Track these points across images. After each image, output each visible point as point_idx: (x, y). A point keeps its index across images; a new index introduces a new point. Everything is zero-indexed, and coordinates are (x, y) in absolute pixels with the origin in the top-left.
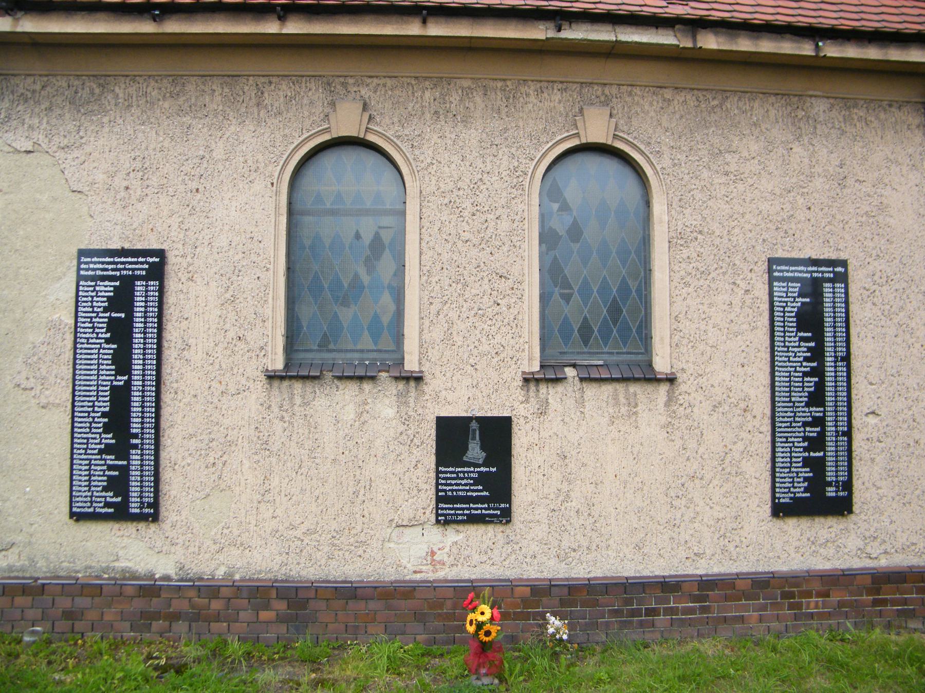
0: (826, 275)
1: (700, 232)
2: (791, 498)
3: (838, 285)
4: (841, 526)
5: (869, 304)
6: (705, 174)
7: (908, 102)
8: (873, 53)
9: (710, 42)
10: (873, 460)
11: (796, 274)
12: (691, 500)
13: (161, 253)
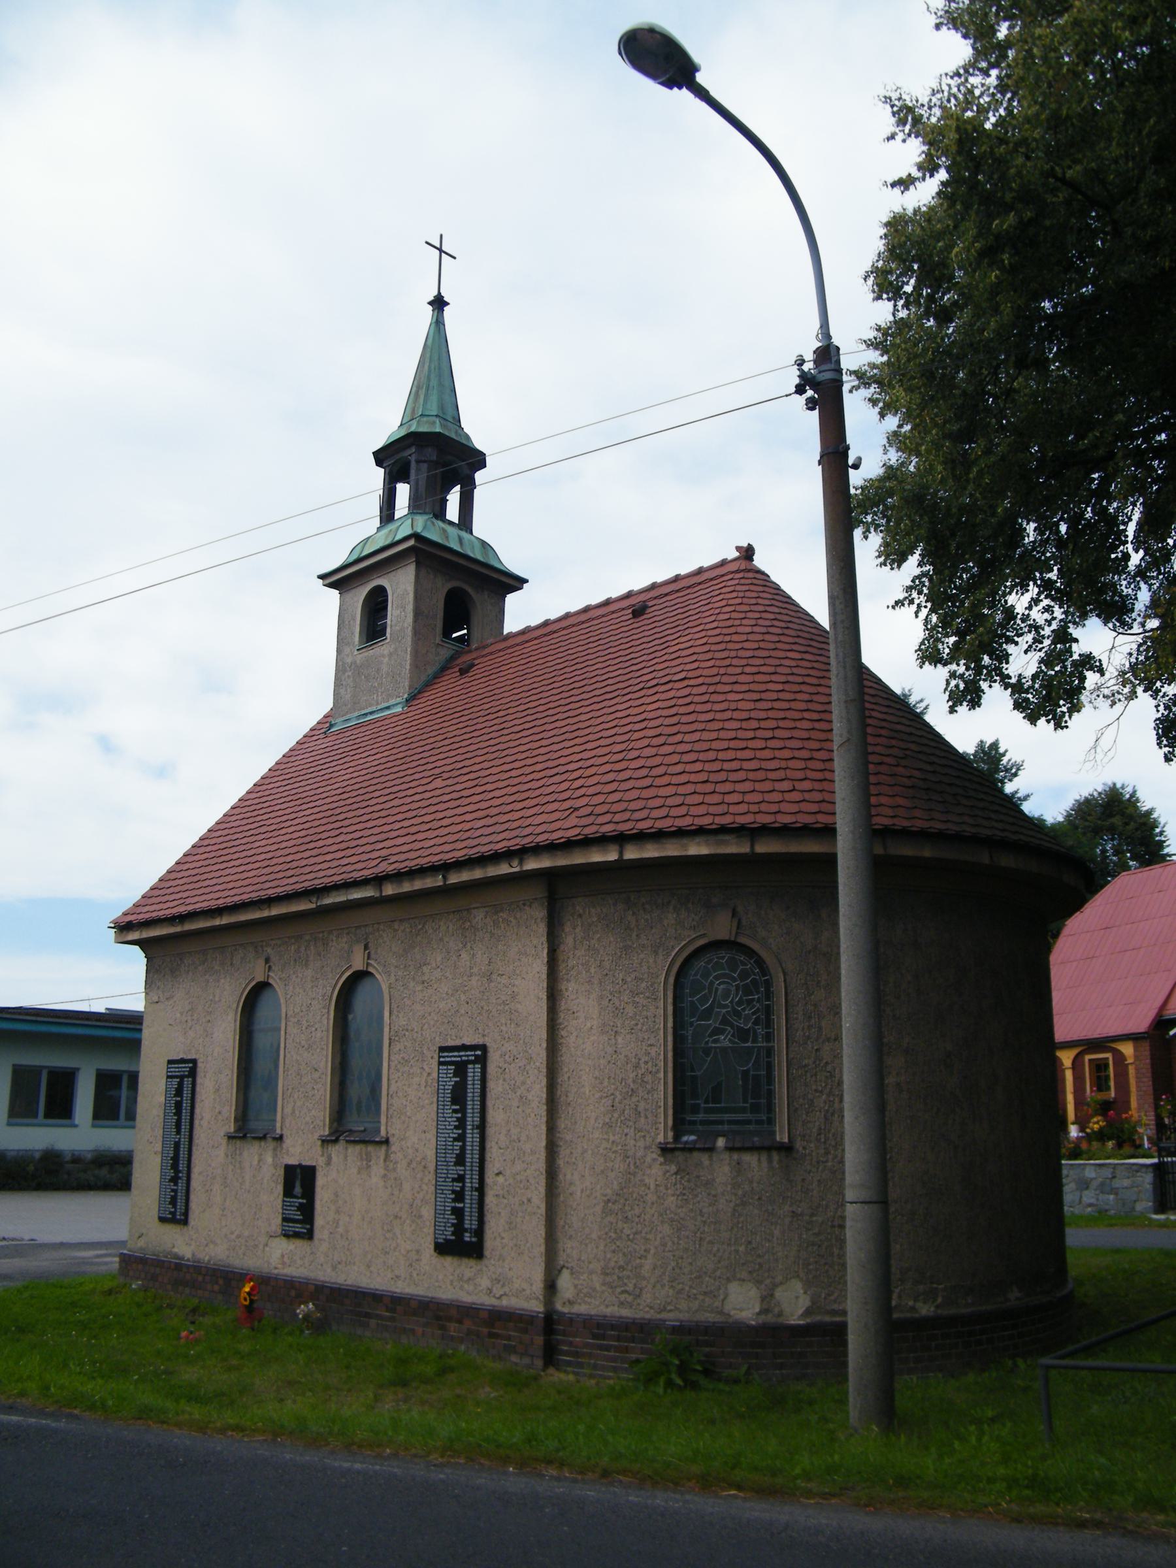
0: (470, 1058)
1: (407, 1030)
2: (445, 1239)
3: (477, 1066)
4: (478, 1268)
5: (501, 1081)
6: (412, 984)
7: (536, 899)
8: (478, 874)
9: (389, 890)
10: (499, 1213)
11: (453, 1059)
12: (394, 1234)
13: (194, 1062)
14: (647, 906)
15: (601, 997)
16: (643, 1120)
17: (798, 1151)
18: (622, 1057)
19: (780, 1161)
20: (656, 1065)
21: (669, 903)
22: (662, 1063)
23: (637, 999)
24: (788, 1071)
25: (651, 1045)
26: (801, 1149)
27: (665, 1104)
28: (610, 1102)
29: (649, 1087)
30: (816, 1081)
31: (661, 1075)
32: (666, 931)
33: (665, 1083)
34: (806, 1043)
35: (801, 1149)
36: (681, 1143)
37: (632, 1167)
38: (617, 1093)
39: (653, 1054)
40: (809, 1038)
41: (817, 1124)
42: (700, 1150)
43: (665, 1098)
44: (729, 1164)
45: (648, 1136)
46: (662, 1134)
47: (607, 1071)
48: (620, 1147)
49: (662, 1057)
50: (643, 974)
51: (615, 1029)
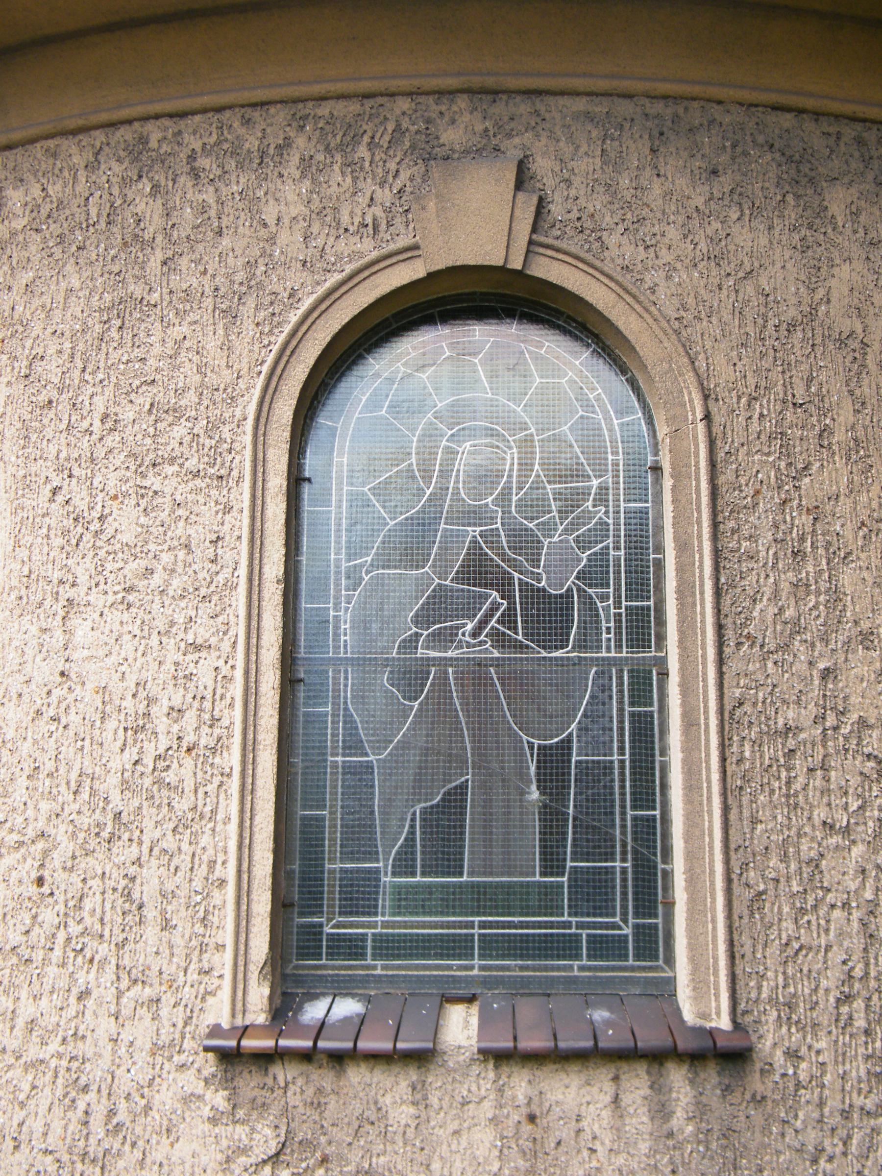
14: (203, 162)
15: (26, 483)
16: (151, 933)
17: (767, 1070)
18: (88, 696)
19: (700, 1111)
20: (215, 721)
21: (287, 144)
22: (238, 713)
23: (153, 481)
24: (723, 747)
25: (197, 647)
26: (779, 1058)
27: (244, 872)
28: (29, 869)
29: (182, 805)
30: (825, 791)
31: (233, 758)
32: (272, 240)
33: (247, 790)
34: (785, 647)
35: (779, 1058)
36: (300, 1031)
37: (98, 1128)
38: (60, 832)
39: (205, 677)
40: (797, 628)
41: (837, 956)
42: (375, 1058)
43: (245, 845)
44: (494, 1121)
45: (168, 999)
46: (225, 993)
47: (26, 748)
48: (54, 1046)
49: (237, 689)
50: (180, 392)
51: (66, 592)
